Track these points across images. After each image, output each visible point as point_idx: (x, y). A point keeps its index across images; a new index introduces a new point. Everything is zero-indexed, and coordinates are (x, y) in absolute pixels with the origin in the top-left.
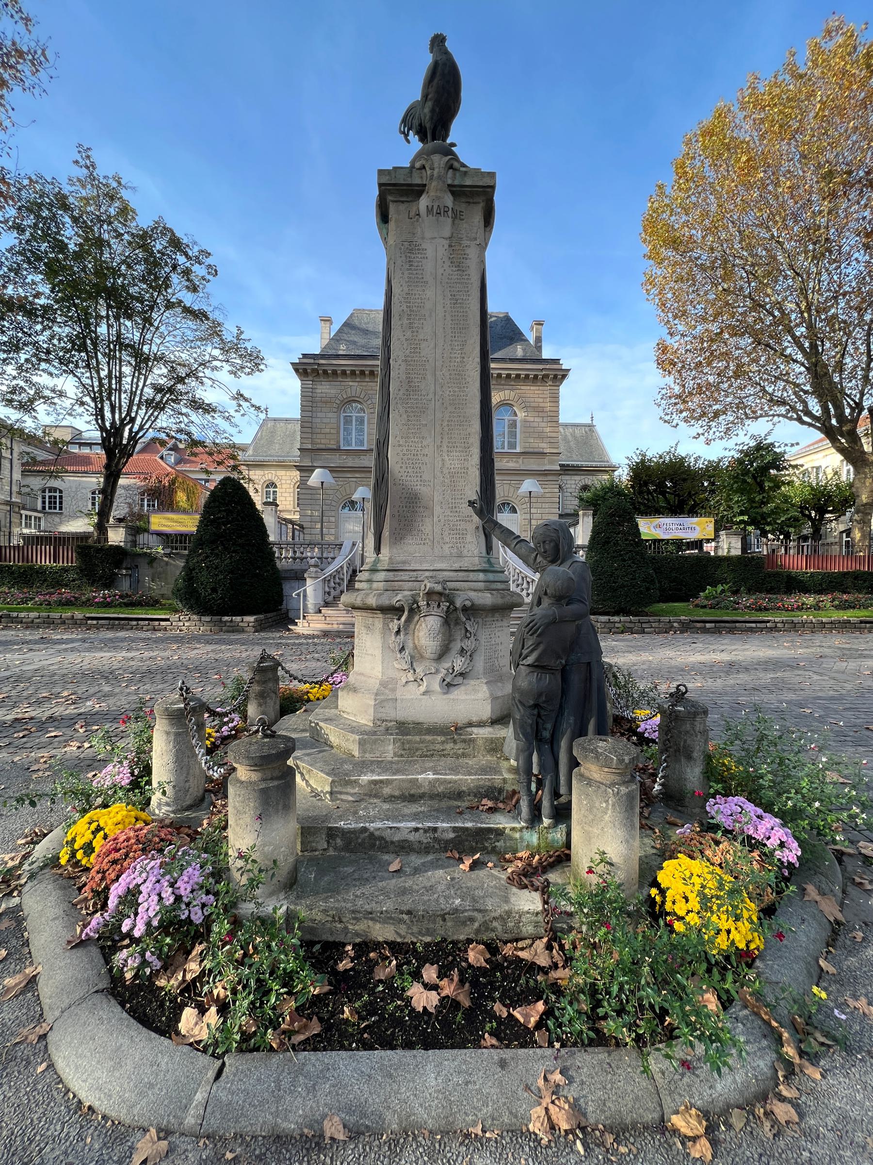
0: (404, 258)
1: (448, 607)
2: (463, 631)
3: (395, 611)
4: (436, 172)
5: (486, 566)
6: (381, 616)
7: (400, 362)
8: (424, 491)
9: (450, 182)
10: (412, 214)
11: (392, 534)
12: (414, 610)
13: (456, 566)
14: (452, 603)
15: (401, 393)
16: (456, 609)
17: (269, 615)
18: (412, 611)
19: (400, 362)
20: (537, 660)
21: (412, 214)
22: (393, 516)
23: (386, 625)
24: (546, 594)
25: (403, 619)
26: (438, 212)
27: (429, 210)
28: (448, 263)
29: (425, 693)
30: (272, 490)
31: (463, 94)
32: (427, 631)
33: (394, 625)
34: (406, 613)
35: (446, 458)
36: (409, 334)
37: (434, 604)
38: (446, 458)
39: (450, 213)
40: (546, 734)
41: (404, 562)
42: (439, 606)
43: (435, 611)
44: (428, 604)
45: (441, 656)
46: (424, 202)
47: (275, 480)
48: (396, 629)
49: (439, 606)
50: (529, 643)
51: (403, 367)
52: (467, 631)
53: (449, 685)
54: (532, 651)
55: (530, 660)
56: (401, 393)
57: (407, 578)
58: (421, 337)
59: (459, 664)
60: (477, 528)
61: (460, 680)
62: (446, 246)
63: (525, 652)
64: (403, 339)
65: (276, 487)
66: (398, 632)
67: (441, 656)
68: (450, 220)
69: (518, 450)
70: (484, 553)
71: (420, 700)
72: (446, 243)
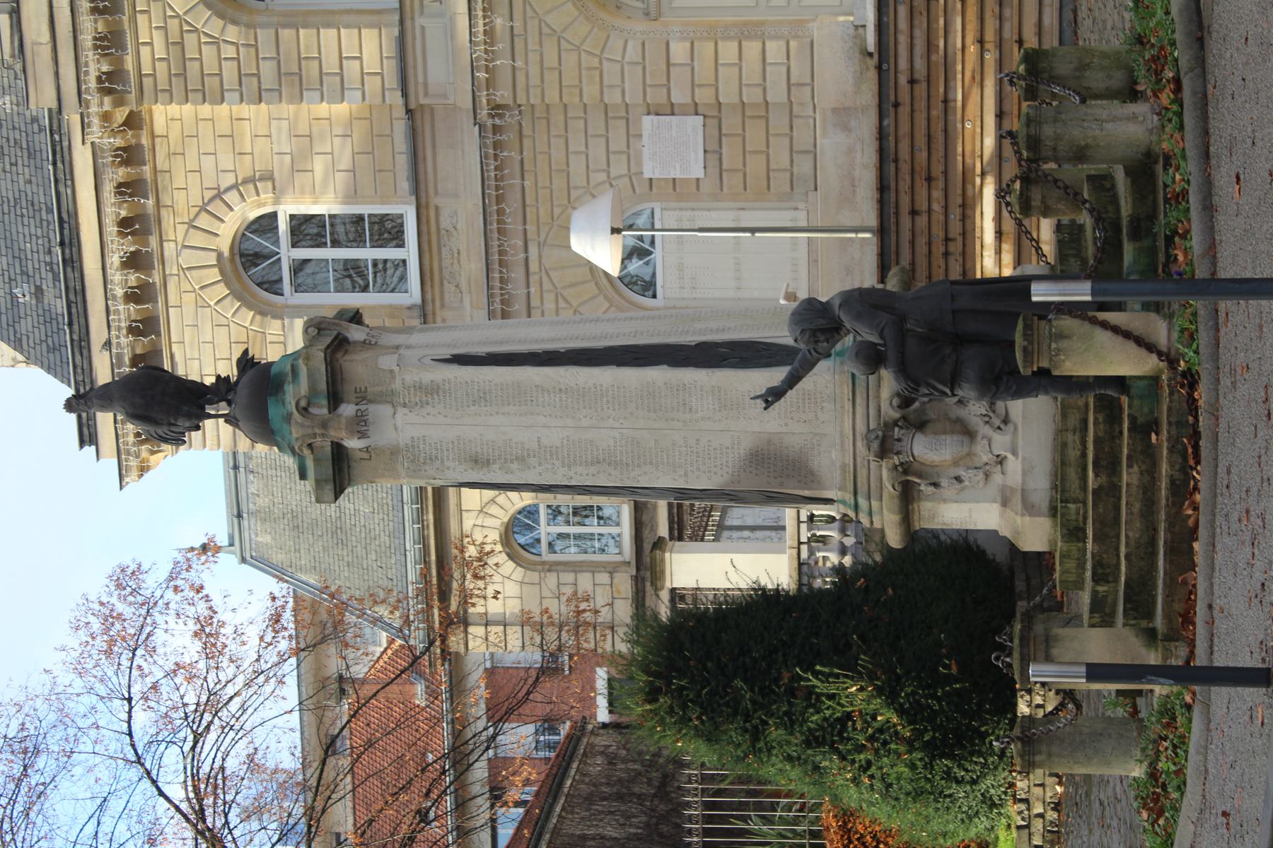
0: (426, 467)
1: (901, 428)
4: (317, 431)
6: (915, 506)
7: (572, 473)
8: (746, 444)
9: (325, 411)
10: (366, 456)
11: (806, 486)
12: (906, 469)
13: (848, 406)
14: (895, 423)
15: (613, 472)
16: (904, 418)
17: (1020, 585)
18: (906, 472)
20: (945, 385)
21: (366, 456)
22: (781, 485)
23: (928, 498)
26: (360, 425)
27: (363, 435)
28: (429, 409)
29: (1014, 453)
30: (288, 254)
34: (910, 478)
35: (700, 414)
36: (533, 461)
37: (897, 446)
38: (700, 414)
39: (363, 408)
42: (899, 440)
43: (906, 443)
44: (898, 453)
45: (968, 433)
46: (353, 444)
47: (227, 230)
48: (931, 489)
49: (899, 440)
51: (580, 469)
53: (1006, 421)
56: (613, 472)
62: (405, 410)
64: (539, 469)
65: (266, 224)
66: (935, 485)
67: (968, 433)
68: (372, 407)
71: (1024, 459)
72: (401, 411)
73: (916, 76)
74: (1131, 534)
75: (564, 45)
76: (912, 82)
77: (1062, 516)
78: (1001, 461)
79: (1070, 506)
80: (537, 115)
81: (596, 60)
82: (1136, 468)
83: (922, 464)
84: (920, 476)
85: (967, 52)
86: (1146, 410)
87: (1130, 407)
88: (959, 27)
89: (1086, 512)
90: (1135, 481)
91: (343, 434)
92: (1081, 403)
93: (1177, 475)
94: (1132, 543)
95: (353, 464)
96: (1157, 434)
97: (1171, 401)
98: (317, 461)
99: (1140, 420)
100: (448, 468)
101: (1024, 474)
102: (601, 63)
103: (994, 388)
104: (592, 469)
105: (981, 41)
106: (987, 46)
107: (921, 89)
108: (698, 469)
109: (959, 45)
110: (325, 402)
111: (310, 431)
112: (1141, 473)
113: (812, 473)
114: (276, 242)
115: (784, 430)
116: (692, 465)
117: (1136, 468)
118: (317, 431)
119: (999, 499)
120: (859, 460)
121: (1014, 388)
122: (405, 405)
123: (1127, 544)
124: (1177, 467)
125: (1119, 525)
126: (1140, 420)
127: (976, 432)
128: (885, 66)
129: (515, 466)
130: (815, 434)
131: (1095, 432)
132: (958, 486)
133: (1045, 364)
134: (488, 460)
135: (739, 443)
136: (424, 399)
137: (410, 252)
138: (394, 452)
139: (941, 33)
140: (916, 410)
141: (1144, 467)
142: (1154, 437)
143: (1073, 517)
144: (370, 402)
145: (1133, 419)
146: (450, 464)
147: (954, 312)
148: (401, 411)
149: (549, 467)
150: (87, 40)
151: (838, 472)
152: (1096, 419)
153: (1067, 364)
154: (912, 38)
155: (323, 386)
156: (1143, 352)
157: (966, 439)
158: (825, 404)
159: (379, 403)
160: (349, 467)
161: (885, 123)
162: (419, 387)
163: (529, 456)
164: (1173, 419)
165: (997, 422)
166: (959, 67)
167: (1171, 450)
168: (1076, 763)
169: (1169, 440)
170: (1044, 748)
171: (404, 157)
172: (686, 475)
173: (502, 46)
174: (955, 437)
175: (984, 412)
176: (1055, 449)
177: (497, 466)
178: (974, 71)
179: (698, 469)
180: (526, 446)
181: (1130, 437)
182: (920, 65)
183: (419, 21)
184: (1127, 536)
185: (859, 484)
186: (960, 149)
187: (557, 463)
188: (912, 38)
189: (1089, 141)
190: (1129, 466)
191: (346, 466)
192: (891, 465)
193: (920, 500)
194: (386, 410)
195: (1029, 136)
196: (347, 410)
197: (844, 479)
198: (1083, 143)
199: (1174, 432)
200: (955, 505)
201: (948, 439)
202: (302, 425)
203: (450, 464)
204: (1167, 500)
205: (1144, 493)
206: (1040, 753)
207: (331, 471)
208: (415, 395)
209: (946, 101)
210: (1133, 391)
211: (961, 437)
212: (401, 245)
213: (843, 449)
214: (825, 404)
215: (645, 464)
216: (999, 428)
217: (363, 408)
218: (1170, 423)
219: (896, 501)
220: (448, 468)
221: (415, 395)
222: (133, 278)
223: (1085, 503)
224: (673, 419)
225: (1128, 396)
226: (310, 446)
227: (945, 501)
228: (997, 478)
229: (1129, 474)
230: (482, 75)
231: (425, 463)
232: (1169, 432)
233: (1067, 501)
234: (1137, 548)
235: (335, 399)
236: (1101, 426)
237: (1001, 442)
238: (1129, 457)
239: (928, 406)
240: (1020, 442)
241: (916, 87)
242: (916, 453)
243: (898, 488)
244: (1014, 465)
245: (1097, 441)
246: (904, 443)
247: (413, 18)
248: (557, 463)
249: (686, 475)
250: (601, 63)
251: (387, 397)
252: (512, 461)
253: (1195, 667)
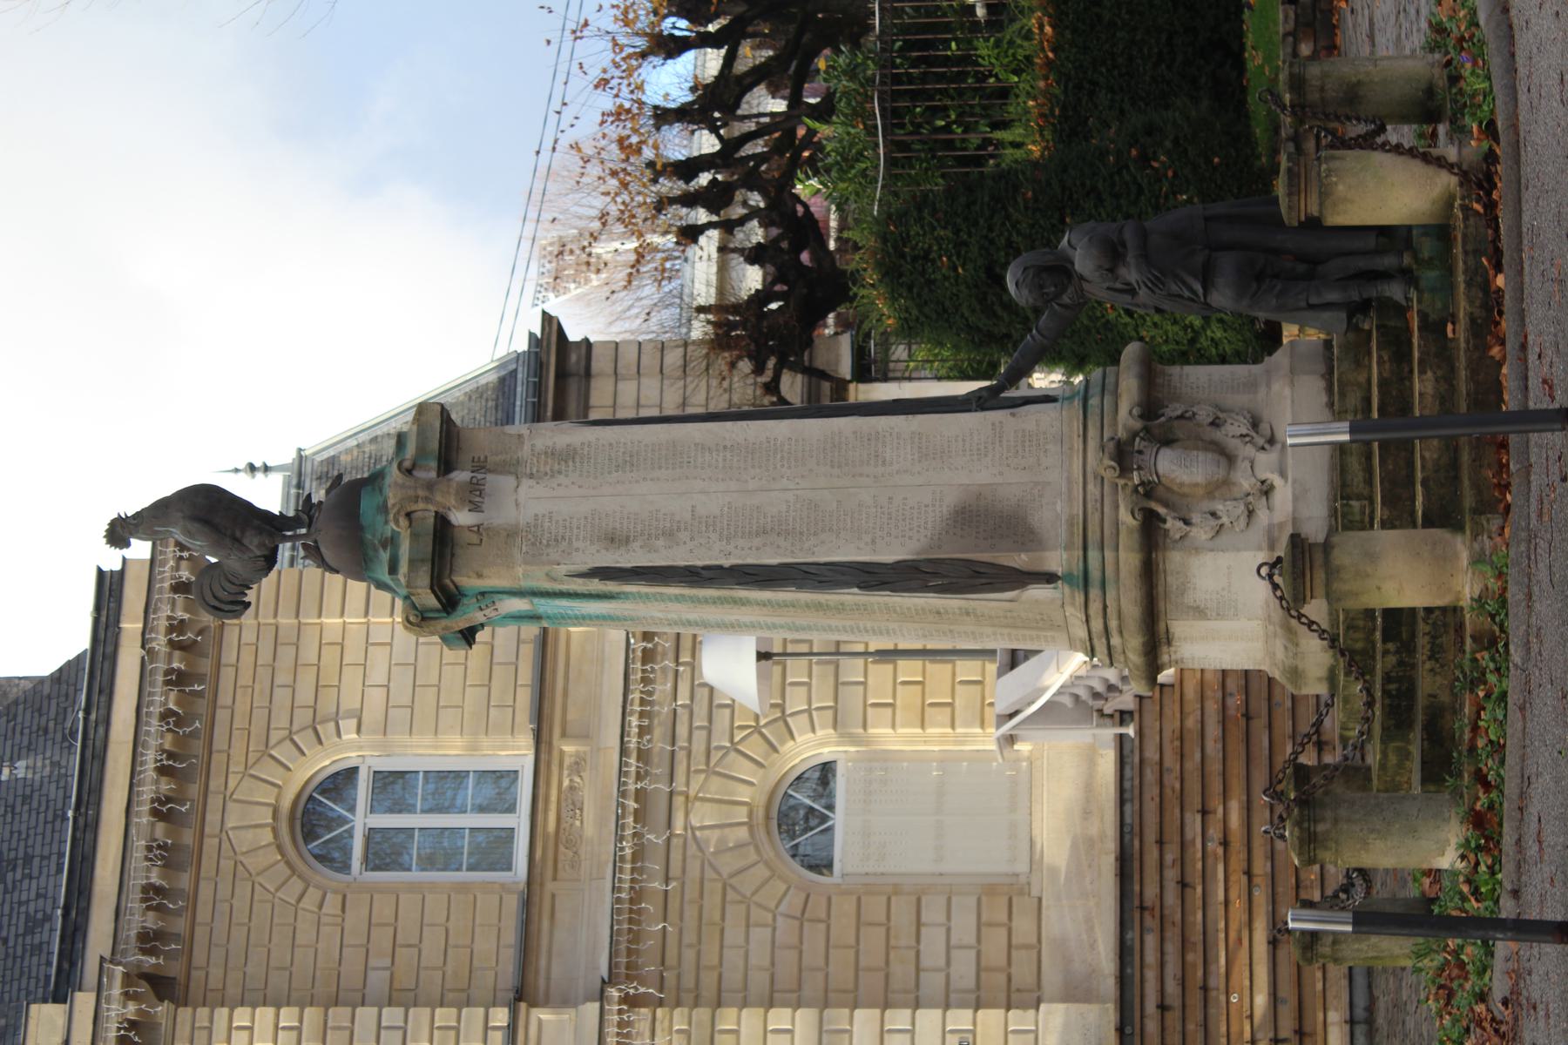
0: (550, 550)
2: (1183, 422)
3: (1151, 533)
4: (421, 493)
5: (1077, 403)
7: (730, 548)
8: (951, 500)
9: (433, 474)
10: (475, 539)
12: (1149, 490)
14: (1135, 435)
18: (1148, 495)
19: (730, 548)
20: (1195, 277)
21: (475, 539)
24: (1111, 270)
25: (1162, 510)
26: (474, 496)
27: (476, 508)
28: (561, 479)
29: (1283, 474)
31: (168, 491)
32: (1177, 468)
33: (1173, 525)
36: (684, 536)
40: (1301, 268)
41: (1071, 524)
42: (1140, 452)
46: (461, 518)
48: (1180, 524)
49: (1140, 452)
50: (1174, 288)
51: (741, 543)
52: (1181, 417)
53: (1272, 441)
54: (1184, 283)
55: (1198, 287)
57: (1097, 516)
58: (688, 516)
59: (1239, 426)
60: (1013, 415)
61: (1264, 427)
62: (532, 482)
63: (1187, 294)
66: (1187, 522)
68: (489, 477)
69: (517, 754)
70: (1058, 405)
71: (1294, 481)
72: (526, 483)
73: (1168, 1001)
74: (1427, 455)
75: (731, 895)
76: (1163, 1007)
77: (1343, 516)
78: (1267, 490)
79: (1353, 503)
80: (696, 724)
81: (770, 916)
82: (1430, 374)
83: (1168, 489)
84: (1166, 505)
85: (1231, 908)
86: (1439, 305)
87: (1419, 301)
88: (1221, 875)
89: (1372, 512)
90: (1429, 388)
91: (452, 501)
92: (1362, 378)
93: (1477, 312)
94: (1430, 465)
95: (458, 551)
96: (1453, 323)
97: (1466, 227)
98: (415, 536)
99: (1433, 317)
100: (577, 550)
101: (1296, 499)
102: (774, 919)
103: (1254, 285)
104: (757, 541)
105: (1249, 873)
106: (1257, 880)
107: (1173, 1018)
108: (889, 534)
109: (1221, 897)
110: (434, 464)
111: (411, 493)
112: (1437, 380)
113: (1032, 532)
114: (352, 809)
115: (999, 480)
116: (881, 528)
117: (1430, 374)
118: (421, 493)
119: (1265, 545)
120: (1089, 506)
121: (1279, 287)
122: (531, 476)
123: (1423, 467)
124: (1478, 303)
125: (1413, 485)
126: (1433, 317)
127: (1236, 456)
128: (1128, 1030)
129: (661, 542)
130: (1037, 484)
131: (1380, 373)
132: (1213, 522)
133: (1314, 210)
134: (628, 538)
135: (941, 500)
136: (556, 467)
137: (519, 822)
138: (512, 533)
139: (1199, 903)
140: (1161, 425)
141: (1439, 373)
142: (1450, 327)
143: (1357, 518)
144: (490, 471)
145: (1423, 316)
146: (580, 544)
147: (1207, 219)
148: (526, 483)
149: (703, 541)
150: (139, 844)
151: (1064, 527)
152: (1380, 357)
153: (1341, 187)
154: (1162, 953)
155: (434, 445)
156: (1430, 170)
157: (1223, 461)
158: (1049, 447)
159: (501, 473)
160: (453, 555)
161: (1129, 936)
162: (552, 453)
163: (679, 529)
164: (1470, 247)
165: (1261, 441)
166: (1222, 925)
167: (1469, 284)
168: (1372, 831)
169: (1465, 272)
170: (1329, 814)
171: (512, 951)
172: (873, 542)
173: (660, 770)
174: (1210, 455)
175: (1245, 431)
176: (1332, 468)
177: (638, 544)
178: (1240, 931)
179: (889, 534)
180: (677, 518)
181: (1420, 337)
182: (1172, 988)
183: (550, 886)
184: (1422, 457)
185: (1090, 534)
186: (1223, 1029)
187: (714, 536)
188: (1162, 953)
189: (1361, 77)
190: (1422, 372)
191: (448, 551)
192: (1128, 491)
193: (1165, 549)
194: (508, 481)
195: (1291, 75)
196: (461, 476)
197: (1072, 534)
198: (1354, 79)
199: (1471, 261)
200: (1210, 555)
201: (1201, 456)
202: (402, 486)
203: (580, 544)
204: (1467, 342)
205: (1441, 404)
206: (1323, 819)
207: (430, 549)
208: (546, 463)
209: (1205, 988)
210: (1423, 283)
211: (1216, 456)
212: (511, 809)
213: (1070, 499)
214: (1049, 447)
215: (823, 531)
216: (1263, 448)
217: (480, 476)
218: (1466, 253)
219: (1136, 536)
220: (577, 550)
221: (546, 463)
222: (166, 786)
223: (1372, 501)
224: (861, 475)
225: (1417, 288)
226: (408, 515)
227: (1197, 550)
228: (1263, 517)
229: (1421, 381)
230: (632, 804)
231: (548, 545)
232: (1465, 263)
233: (1349, 498)
234: (1437, 471)
235: (446, 465)
236: (1387, 366)
237: (1265, 464)
238: (1421, 362)
239: (1176, 423)
240: (1290, 461)
241: (1168, 1015)
242: (1161, 471)
243: (1139, 516)
244: (1283, 494)
245: (1383, 384)
246: (1146, 457)
247: (542, 885)
248: (714, 536)
249: (873, 542)
250: (774, 919)
251: (511, 467)
252: (657, 538)
253: (1507, 412)
